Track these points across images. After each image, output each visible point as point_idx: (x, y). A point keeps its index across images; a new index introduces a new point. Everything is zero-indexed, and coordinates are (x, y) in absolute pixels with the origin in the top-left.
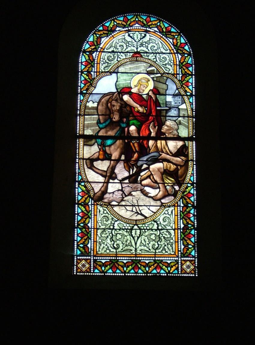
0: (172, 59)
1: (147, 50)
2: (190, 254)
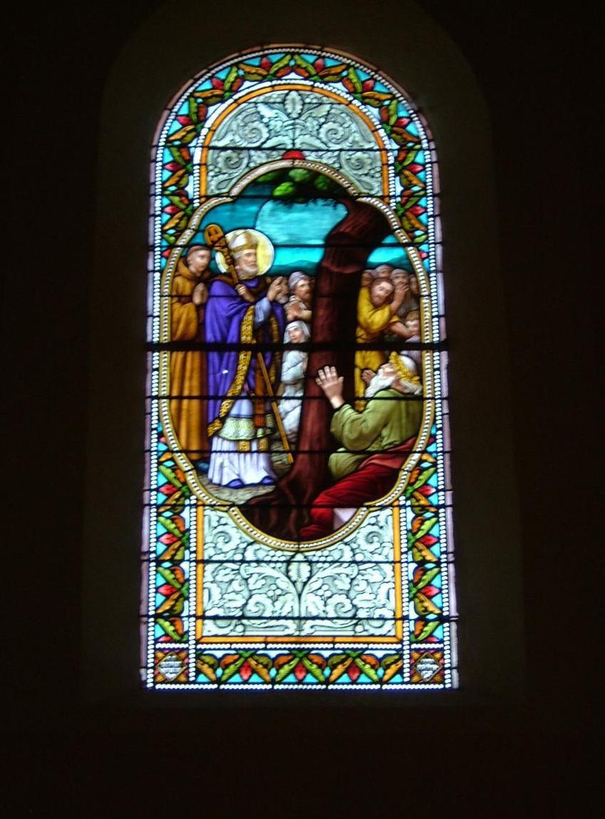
1: (318, 144)
2: (431, 635)
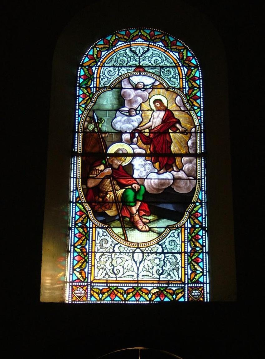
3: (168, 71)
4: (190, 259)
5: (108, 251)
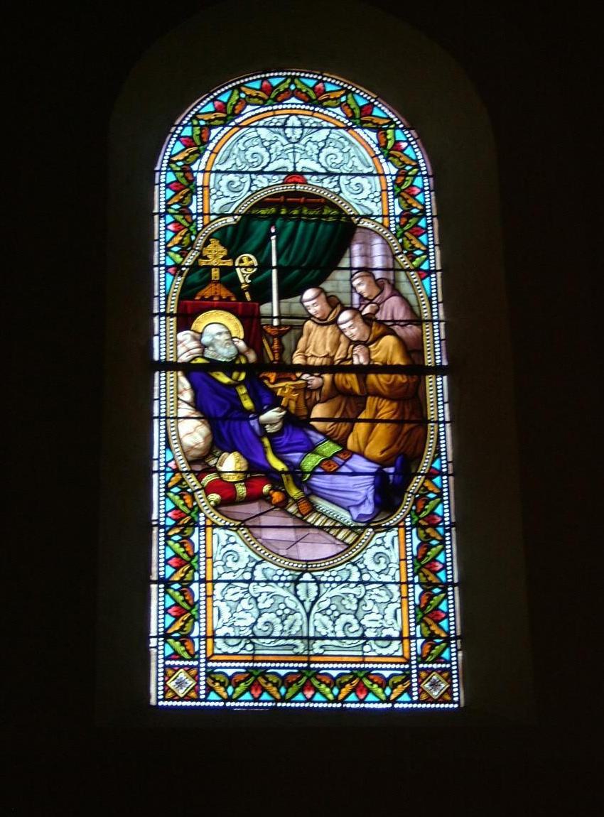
0: (326, 653)
3: (360, 187)
4: (420, 613)
5: (241, 578)
